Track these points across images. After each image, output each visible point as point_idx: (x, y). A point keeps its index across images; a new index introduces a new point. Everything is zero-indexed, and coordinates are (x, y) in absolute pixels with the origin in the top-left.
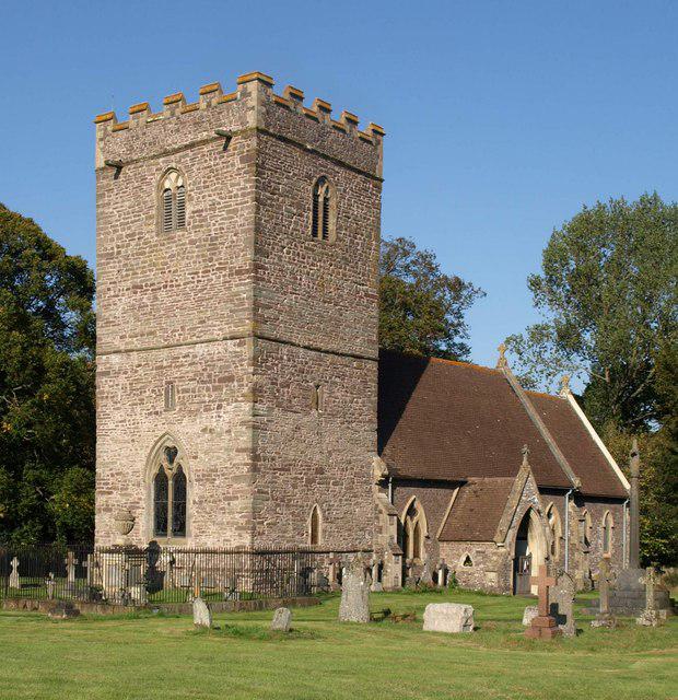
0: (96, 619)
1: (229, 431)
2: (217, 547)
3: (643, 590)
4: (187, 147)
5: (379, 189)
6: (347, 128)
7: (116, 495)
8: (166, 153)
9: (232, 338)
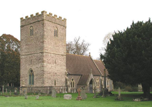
0: (85, 100)
1: (40, 68)
2: (38, 86)
3: (136, 90)
4: (34, 23)
5: (66, 28)
6: (60, 19)
7: (23, 78)
8: (31, 24)
9: (40, 53)
